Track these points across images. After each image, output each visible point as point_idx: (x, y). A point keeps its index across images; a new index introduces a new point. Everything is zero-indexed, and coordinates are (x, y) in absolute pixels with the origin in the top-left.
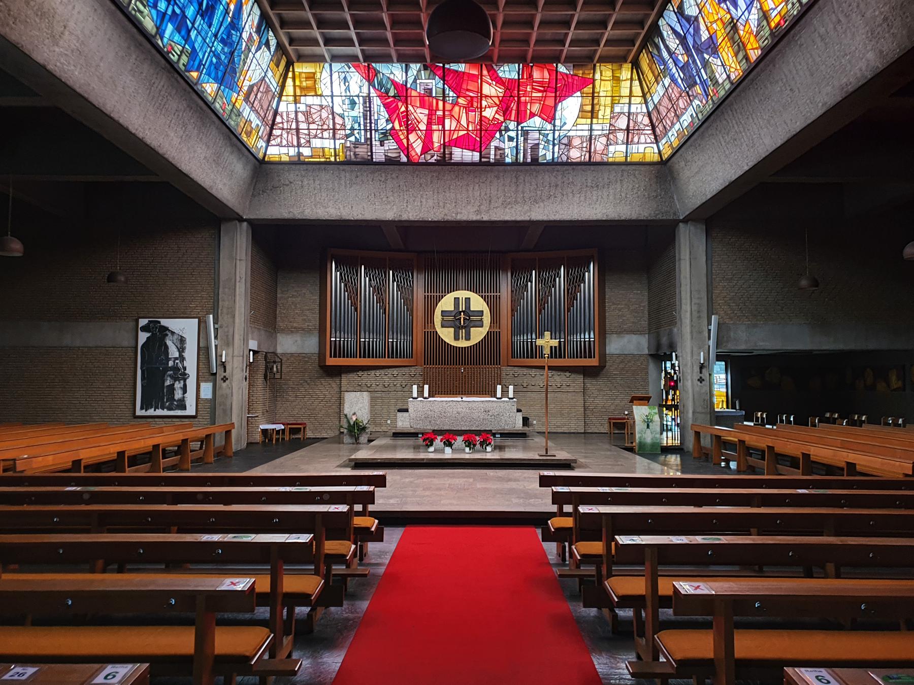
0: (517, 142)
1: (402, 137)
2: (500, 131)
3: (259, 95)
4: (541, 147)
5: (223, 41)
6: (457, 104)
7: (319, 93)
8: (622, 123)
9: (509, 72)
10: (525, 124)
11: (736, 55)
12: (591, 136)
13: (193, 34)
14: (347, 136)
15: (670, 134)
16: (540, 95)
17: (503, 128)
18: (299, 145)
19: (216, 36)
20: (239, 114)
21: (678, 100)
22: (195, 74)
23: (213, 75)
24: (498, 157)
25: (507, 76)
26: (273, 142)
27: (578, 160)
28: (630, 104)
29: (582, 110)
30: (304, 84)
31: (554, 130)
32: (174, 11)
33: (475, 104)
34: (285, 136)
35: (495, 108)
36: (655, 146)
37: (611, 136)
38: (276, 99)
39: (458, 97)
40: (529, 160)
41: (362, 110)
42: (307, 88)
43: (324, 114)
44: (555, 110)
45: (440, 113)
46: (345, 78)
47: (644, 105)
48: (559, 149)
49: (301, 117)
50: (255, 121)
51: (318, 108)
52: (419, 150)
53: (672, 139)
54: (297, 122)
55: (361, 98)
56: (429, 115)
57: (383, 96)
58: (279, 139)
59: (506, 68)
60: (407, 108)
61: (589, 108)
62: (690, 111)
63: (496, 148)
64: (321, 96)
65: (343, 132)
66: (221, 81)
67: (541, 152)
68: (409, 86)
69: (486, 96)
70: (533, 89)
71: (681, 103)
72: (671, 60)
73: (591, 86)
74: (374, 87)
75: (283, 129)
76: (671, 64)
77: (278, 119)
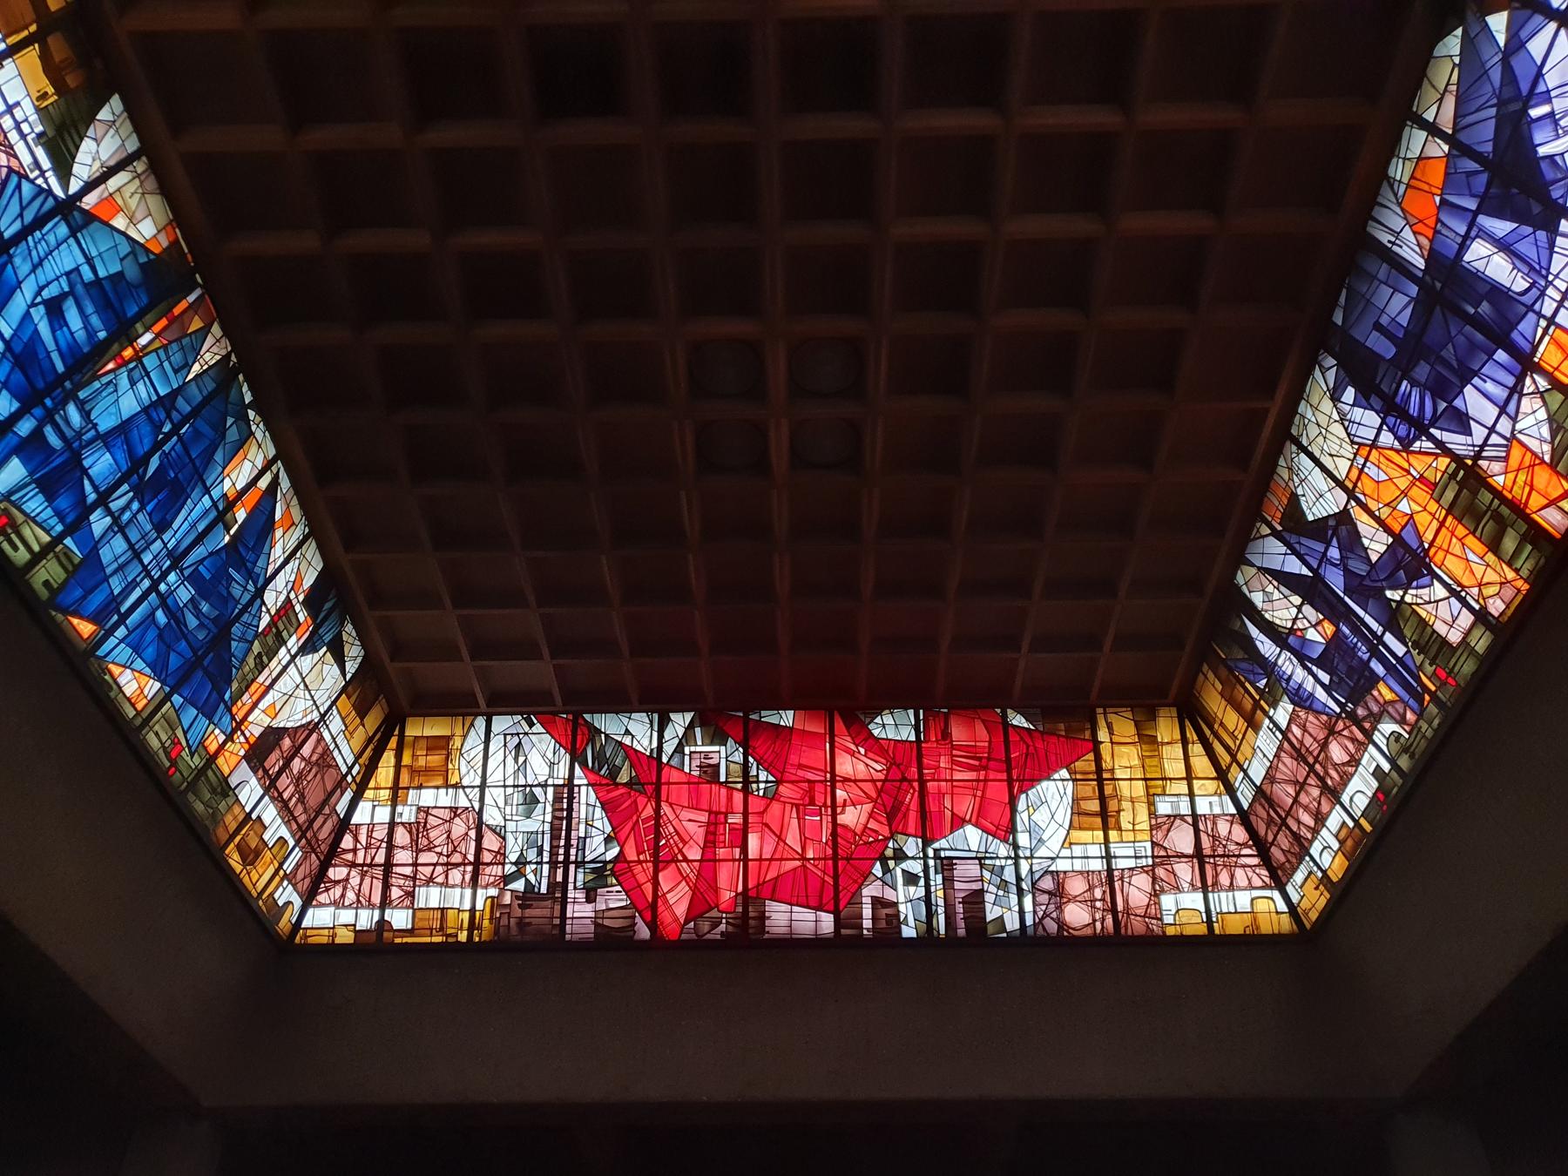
0: (927, 886)
1: (642, 878)
2: (884, 860)
3: (297, 765)
4: (989, 898)
5: (194, 579)
6: (776, 797)
7: (454, 780)
8: (1182, 840)
9: (895, 727)
10: (943, 843)
11: (1494, 546)
12: (1110, 871)
13: (99, 523)
14: (507, 879)
15: (1315, 850)
16: (971, 775)
17: (889, 853)
18: (385, 902)
19: (177, 558)
20: (225, 790)
21: (1324, 746)
22: (86, 628)
23: (150, 652)
24: (883, 924)
25: (891, 734)
26: (322, 898)
27: (1089, 931)
28: (1191, 795)
29: (1077, 811)
30: (422, 762)
31: (1017, 857)
32: (37, 433)
33: (819, 800)
34: (355, 881)
35: (868, 807)
36: (1276, 895)
37: (1160, 872)
38: (348, 795)
39: (778, 782)
40: (961, 932)
41: (548, 818)
42: (428, 771)
43: (459, 828)
44: (1013, 811)
45: (735, 819)
46: (519, 744)
47: (1227, 799)
48: (1035, 904)
49: (401, 837)
50: (276, 828)
51: (446, 814)
52: (681, 910)
53: (1326, 860)
54: (391, 847)
55: (550, 790)
56: (709, 824)
57: (604, 783)
58: (338, 891)
59: (888, 719)
60: (657, 809)
61: (1094, 806)
62: (1373, 758)
63: (877, 902)
64: (455, 786)
65: (497, 870)
66: (174, 682)
67: (992, 913)
68: (665, 760)
69: (846, 780)
70: (953, 762)
71: (1337, 753)
72: (1286, 654)
73: (1091, 756)
74: (584, 765)
75: (353, 865)
76: (1287, 664)
77: (347, 842)
